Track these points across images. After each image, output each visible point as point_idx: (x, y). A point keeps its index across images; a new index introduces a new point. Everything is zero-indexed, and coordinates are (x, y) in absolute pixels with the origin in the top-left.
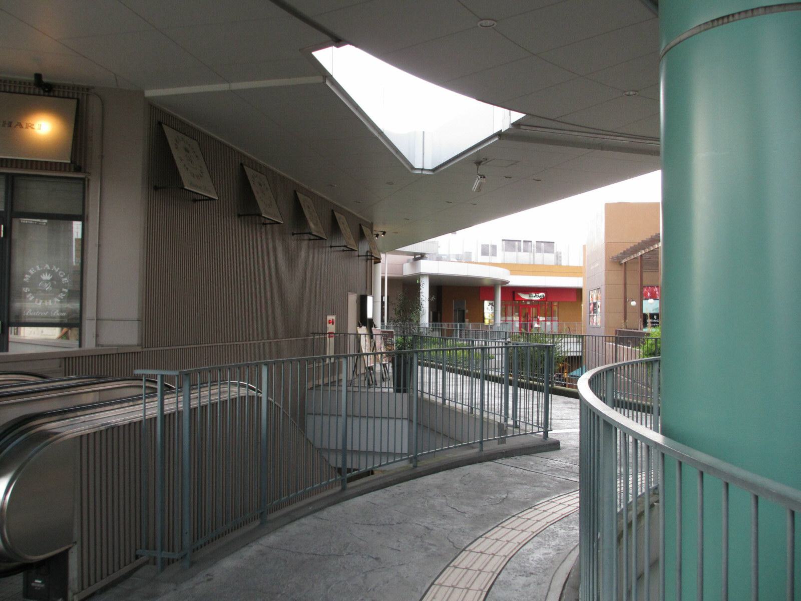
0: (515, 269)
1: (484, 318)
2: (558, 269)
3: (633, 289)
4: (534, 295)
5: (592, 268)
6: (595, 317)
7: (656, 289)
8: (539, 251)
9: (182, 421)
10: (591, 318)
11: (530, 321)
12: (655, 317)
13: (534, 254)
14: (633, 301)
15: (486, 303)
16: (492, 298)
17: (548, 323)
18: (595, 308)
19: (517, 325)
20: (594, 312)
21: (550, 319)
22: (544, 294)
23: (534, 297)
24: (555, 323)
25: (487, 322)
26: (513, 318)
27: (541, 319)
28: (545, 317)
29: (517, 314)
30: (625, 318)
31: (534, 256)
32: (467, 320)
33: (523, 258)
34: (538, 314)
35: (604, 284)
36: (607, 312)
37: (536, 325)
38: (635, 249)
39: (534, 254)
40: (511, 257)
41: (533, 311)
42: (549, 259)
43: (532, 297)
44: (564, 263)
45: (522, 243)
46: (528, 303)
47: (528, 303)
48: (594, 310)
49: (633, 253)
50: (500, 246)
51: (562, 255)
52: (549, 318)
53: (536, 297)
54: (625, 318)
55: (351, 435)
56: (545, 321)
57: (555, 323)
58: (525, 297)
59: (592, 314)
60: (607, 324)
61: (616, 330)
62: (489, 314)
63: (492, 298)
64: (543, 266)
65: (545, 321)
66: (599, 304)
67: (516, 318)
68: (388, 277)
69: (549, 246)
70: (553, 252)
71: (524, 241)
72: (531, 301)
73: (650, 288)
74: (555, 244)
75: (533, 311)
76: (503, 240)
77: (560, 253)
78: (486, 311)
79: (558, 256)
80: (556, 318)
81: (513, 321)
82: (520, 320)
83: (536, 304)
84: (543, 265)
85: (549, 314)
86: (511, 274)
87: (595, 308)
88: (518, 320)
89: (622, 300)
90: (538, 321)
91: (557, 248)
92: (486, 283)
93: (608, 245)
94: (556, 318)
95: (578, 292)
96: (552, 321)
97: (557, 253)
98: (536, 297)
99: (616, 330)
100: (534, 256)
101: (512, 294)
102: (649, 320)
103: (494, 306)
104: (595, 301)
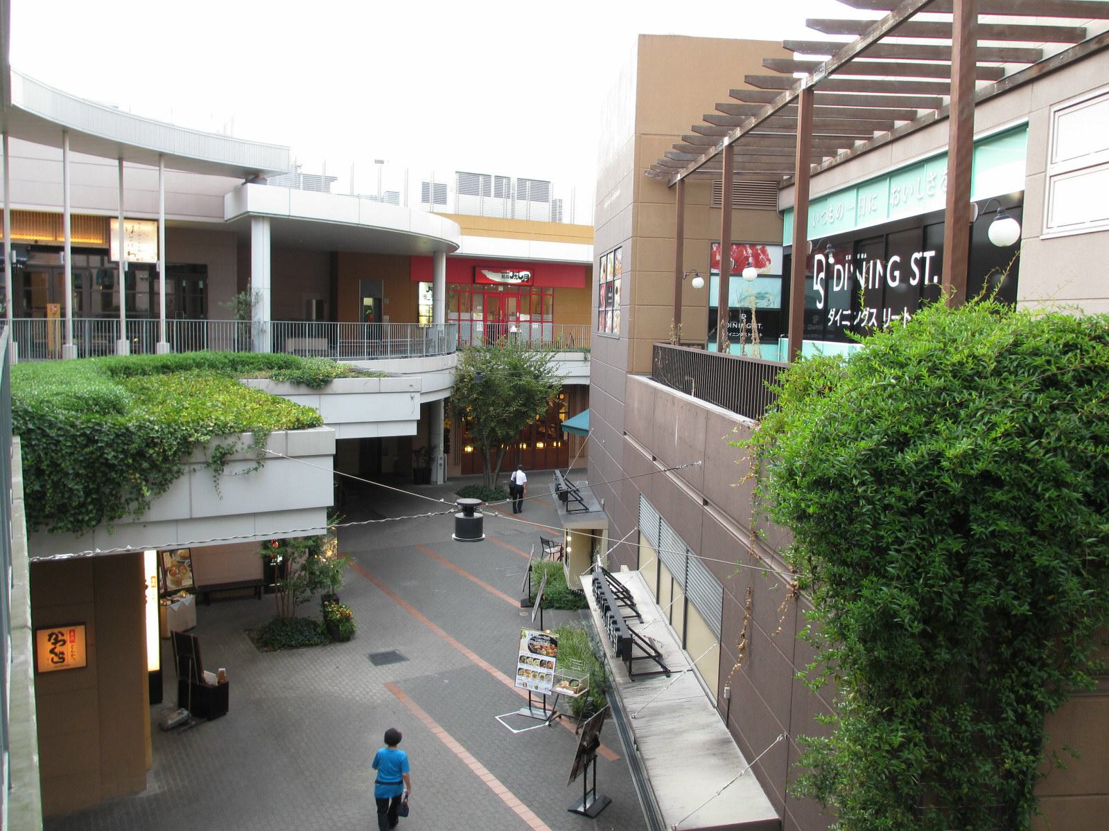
0: (470, 224)
1: (418, 315)
2: (555, 230)
3: (695, 252)
4: (511, 274)
5: (606, 205)
6: (610, 314)
7: (750, 251)
8: (522, 196)
9: (874, 244)
10: (602, 315)
11: (503, 321)
12: (743, 317)
13: (513, 200)
14: (697, 276)
15: (423, 287)
16: (431, 278)
17: (535, 326)
18: (610, 295)
19: (480, 327)
20: (607, 304)
21: (540, 319)
22: (528, 273)
23: (512, 278)
24: (547, 326)
25: (423, 321)
26: (472, 316)
27: (523, 317)
28: (530, 313)
29: (480, 308)
30: (678, 319)
31: (513, 205)
32: (386, 318)
33: (493, 206)
34: (519, 309)
35: (630, 269)
36: (636, 304)
37: (513, 329)
38: (709, 135)
39: (513, 200)
40: (471, 204)
41: (512, 303)
42: (540, 211)
43: (507, 277)
44: (566, 220)
45: (493, 180)
46: (501, 289)
47: (501, 289)
48: (607, 298)
49: (703, 149)
50: (452, 183)
51: (564, 205)
52: (538, 317)
53: (514, 279)
54: (678, 319)
55: (401, 426)
56: (530, 321)
57: (547, 326)
58: (495, 277)
59: (602, 309)
60: (633, 331)
61: (655, 348)
62: (427, 308)
63: (431, 278)
64: (528, 222)
65: (530, 321)
66: (618, 284)
67: (478, 316)
68: (166, 221)
69: (539, 190)
70: (547, 201)
71: (496, 177)
72: (505, 284)
73: (734, 247)
74: (550, 186)
75: (512, 303)
76: (457, 172)
77: (560, 201)
78: (422, 301)
79: (556, 208)
80: (550, 317)
81: (472, 320)
82: (485, 320)
83: (517, 291)
84: (528, 221)
85: (538, 311)
86: (462, 234)
87: (610, 295)
88: (481, 318)
89: (673, 276)
90: (518, 320)
91: (556, 193)
92: (423, 248)
93: (642, 138)
94: (550, 317)
95: (585, 270)
96: (542, 322)
97: (554, 202)
98: (514, 279)
99: (655, 348)
100: (513, 205)
101: (469, 273)
102: (722, 323)
103: (433, 289)
104: (610, 278)
